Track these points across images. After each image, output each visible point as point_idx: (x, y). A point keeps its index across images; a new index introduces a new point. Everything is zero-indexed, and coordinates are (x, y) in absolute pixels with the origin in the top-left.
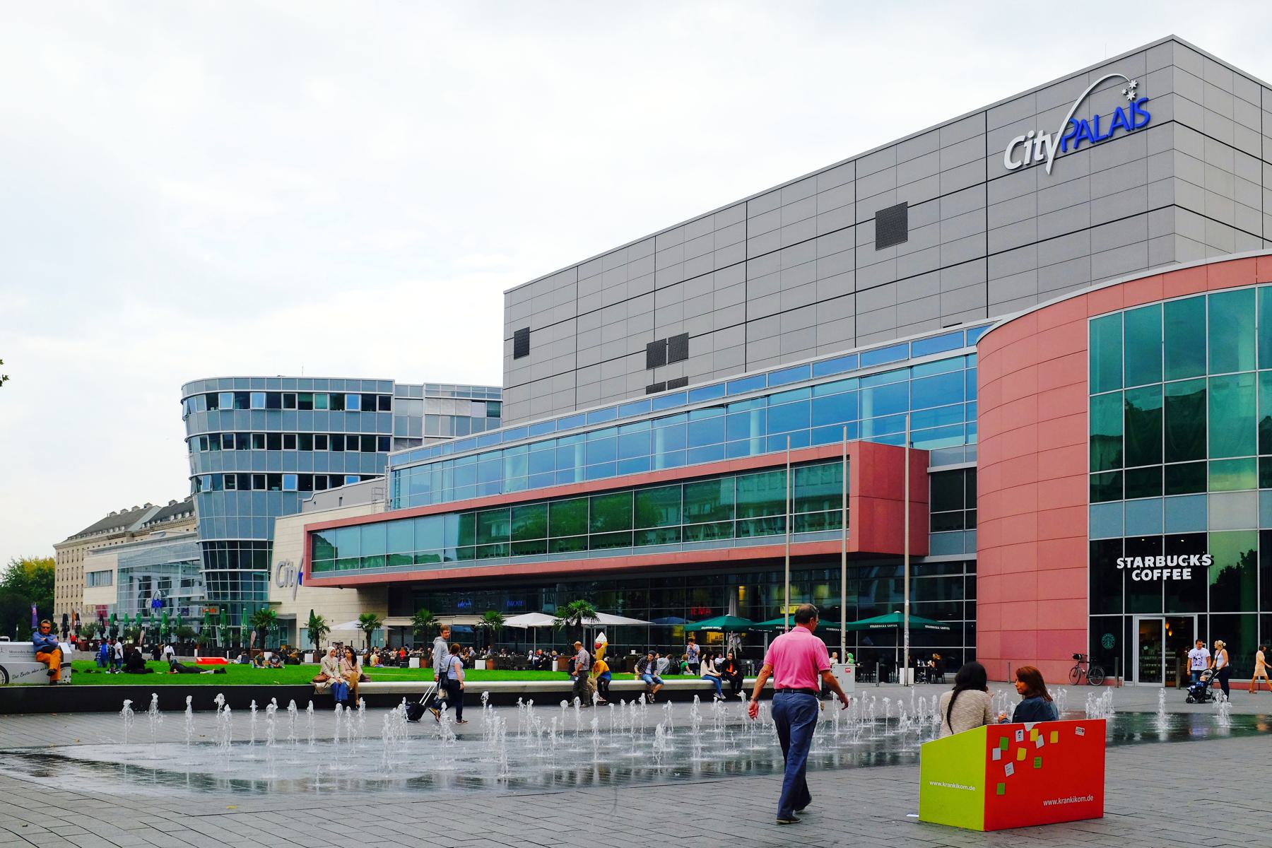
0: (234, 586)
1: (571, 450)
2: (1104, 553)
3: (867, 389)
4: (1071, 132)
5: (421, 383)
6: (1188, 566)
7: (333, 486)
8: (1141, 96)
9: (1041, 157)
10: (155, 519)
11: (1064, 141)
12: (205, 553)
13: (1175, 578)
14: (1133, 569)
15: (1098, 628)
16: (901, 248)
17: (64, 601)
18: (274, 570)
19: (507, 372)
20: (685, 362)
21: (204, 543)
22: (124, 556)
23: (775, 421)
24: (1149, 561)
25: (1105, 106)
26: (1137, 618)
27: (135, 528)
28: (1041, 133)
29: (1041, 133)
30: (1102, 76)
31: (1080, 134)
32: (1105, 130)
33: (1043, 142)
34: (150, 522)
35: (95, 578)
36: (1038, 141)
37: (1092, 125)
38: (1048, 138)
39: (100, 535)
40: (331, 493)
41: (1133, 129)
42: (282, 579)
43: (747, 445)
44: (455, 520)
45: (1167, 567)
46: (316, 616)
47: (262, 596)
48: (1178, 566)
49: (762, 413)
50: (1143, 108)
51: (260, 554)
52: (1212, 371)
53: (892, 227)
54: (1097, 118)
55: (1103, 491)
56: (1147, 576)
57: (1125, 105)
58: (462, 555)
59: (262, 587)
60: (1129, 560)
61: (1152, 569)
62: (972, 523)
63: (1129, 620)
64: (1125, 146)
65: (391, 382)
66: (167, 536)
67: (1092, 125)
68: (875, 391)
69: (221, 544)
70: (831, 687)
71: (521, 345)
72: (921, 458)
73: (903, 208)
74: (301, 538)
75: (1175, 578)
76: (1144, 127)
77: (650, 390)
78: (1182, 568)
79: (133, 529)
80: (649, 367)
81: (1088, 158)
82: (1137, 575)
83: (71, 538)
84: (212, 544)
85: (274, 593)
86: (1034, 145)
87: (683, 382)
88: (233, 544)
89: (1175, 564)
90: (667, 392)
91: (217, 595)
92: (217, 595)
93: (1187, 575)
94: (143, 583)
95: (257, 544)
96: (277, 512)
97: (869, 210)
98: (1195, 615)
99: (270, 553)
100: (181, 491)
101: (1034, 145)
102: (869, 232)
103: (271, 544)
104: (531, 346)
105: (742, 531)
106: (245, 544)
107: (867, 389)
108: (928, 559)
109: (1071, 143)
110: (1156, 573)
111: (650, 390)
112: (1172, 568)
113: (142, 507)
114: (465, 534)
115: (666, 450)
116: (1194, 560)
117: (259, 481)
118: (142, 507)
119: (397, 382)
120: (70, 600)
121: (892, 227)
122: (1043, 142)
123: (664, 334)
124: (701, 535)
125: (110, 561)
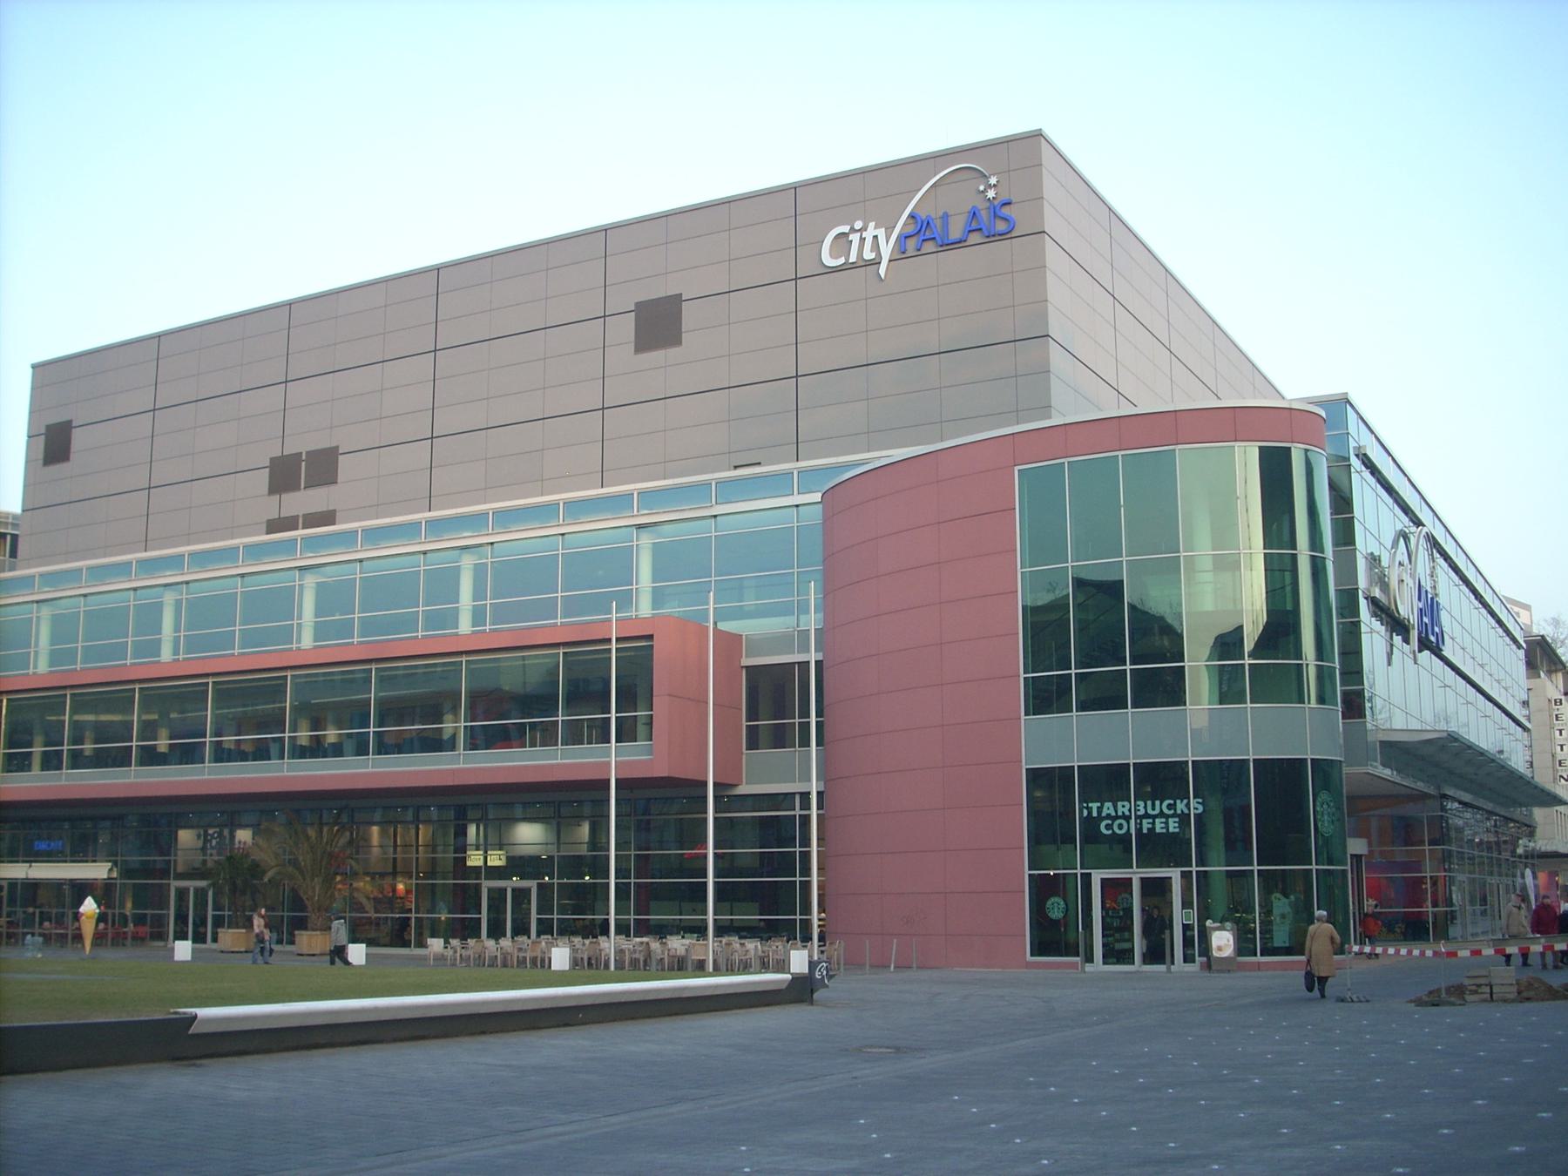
2: (1050, 787)
4: (911, 229)
7: (142, 763)
8: (1004, 197)
9: (873, 256)
13: (1158, 830)
14: (1100, 818)
15: (1043, 889)
16: (673, 352)
19: (31, 484)
20: (333, 488)
25: (959, 204)
26: (1097, 876)
28: (872, 225)
29: (872, 225)
31: (924, 234)
33: (876, 237)
36: (869, 235)
38: (881, 233)
41: (993, 237)
43: (455, 614)
45: (1146, 815)
48: (1162, 814)
49: (479, 571)
50: (1006, 211)
53: (659, 324)
54: (945, 217)
55: (1045, 698)
57: (982, 206)
60: (1094, 806)
63: (1087, 879)
64: (977, 258)
67: (939, 223)
68: (321, 588)
70: (95, 840)
71: (53, 444)
72: (729, 644)
73: (676, 300)
75: (1158, 830)
76: (1003, 236)
77: (274, 526)
78: (1167, 817)
80: (272, 491)
82: (1108, 827)
86: (862, 240)
87: (328, 518)
89: (1157, 811)
93: (1173, 826)
97: (625, 299)
98: (1174, 874)
101: (862, 240)
107: (646, 541)
108: (743, 789)
109: (911, 244)
115: (317, 616)
116: (1180, 806)
121: (659, 324)
122: (876, 237)
123: (302, 443)
124: (36, 761)
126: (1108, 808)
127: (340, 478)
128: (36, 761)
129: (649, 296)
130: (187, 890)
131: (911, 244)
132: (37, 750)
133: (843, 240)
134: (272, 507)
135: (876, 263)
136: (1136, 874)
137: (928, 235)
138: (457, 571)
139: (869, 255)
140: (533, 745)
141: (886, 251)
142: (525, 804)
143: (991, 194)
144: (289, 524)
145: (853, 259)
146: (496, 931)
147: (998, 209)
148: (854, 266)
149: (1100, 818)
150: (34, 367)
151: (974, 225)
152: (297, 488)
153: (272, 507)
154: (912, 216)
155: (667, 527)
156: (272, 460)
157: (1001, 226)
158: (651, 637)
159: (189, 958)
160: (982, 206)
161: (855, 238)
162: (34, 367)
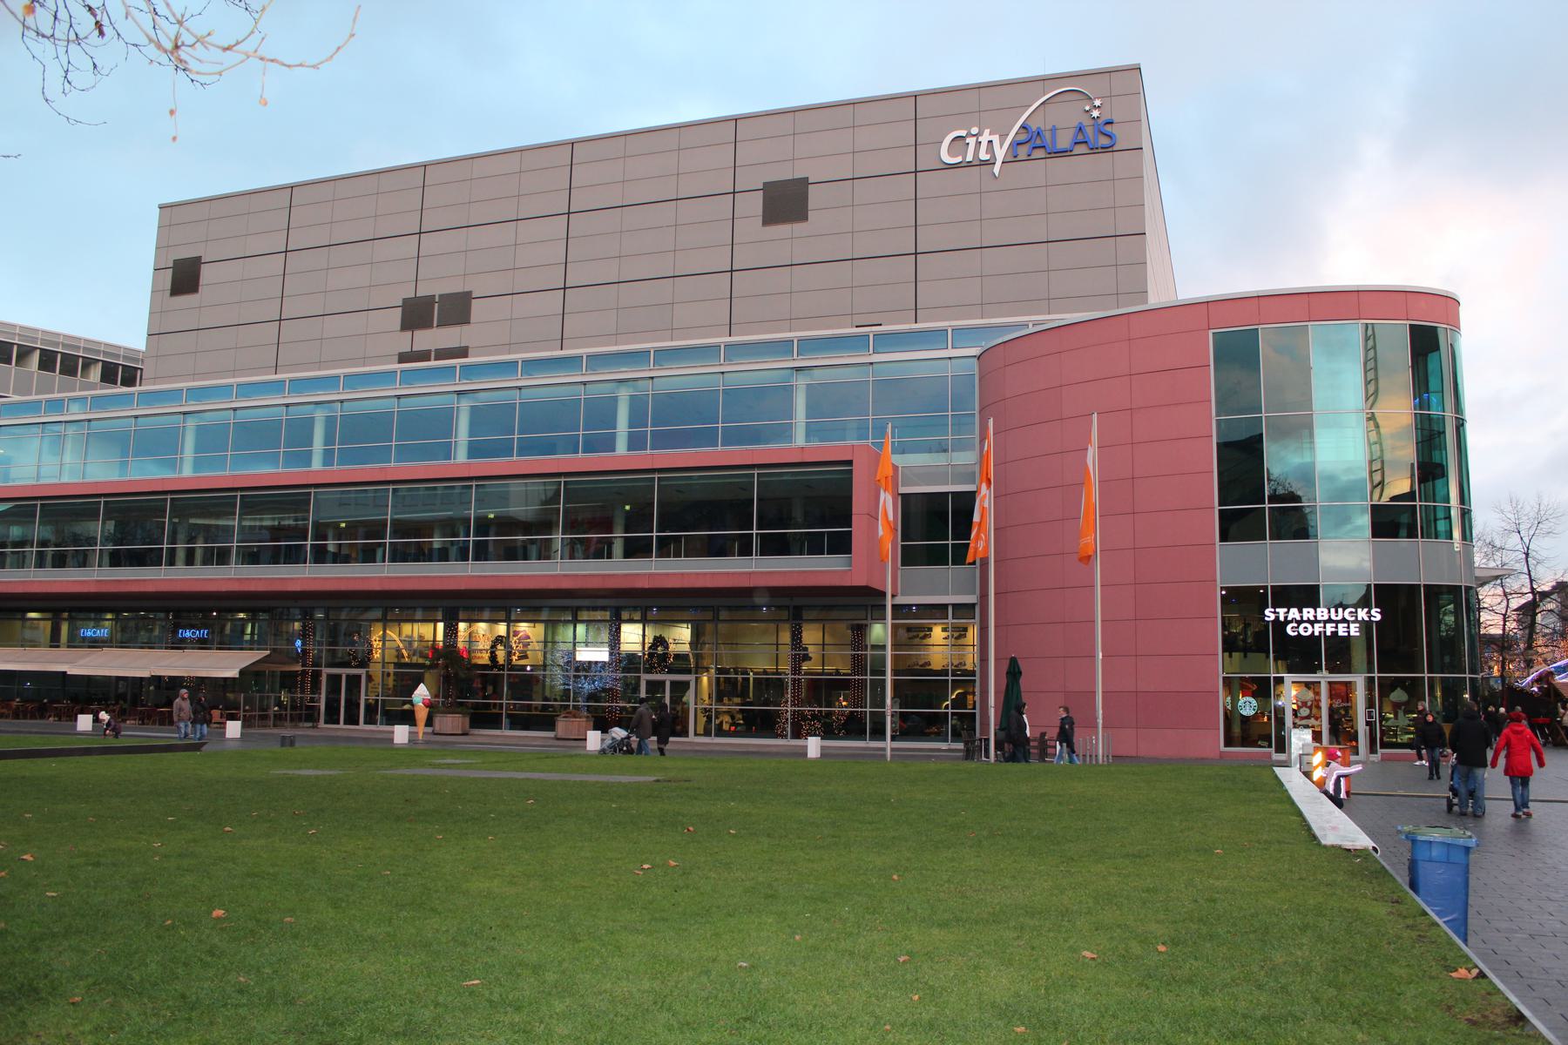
1: (310, 423)
3: (465, 405)
4: (1023, 137)
6: (1356, 621)
8: (1106, 117)
9: (987, 157)
11: (1016, 144)
14: (1287, 622)
16: (798, 227)
20: (465, 328)
23: (210, 439)
24: (1308, 613)
25: (1065, 120)
28: (987, 131)
29: (987, 131)
30: (1072, 87)
31: (1033, 143)
32: (1064, 142)
36: (984, 139)
37: (1048, 135)
38: (996, 139)
41: (1094, 150)
43: (613, 438)
45: (1330, 620)
48: (1344, 620)
49: (330, 421)
50: (1108, 129)
53: (786, 202)
54: (1054, 130)
56: (1305, 631)
60: (1282, 611)
61: (1312, 623)
62: (572, 557)
64: (1083, 165)
68: (474, 410)
71: (184, 278)
73: (805, 182)
77: (403, 358)
80: (404, 327)
81: (1039, 169)
87: (463, 352)
90: (433, 363)
93: (1354, 630)
102: (755, 204)
104: (811, 206)
107: (465, 405)
110: (1330, 629)
111: (403, 358)
112: (1337, 622)
121: (786, 202)
123: (435, 287)
124: (618, 548)
126: (1294, 613)
127: (473, 320)
128: (618, 548)
129: (779, 180)
130: (340, 676)
131: (1023, 152)
132: (618, 535)
133: (960, 143)
134: (404, 342)
135: (990, 163)
136: (668, 678)
137: (1038, 142)
138: (615, 399)
139: (984, 156)
140: (678, 555)
141: (1000, 154)
142: (425, 609)
143: (1095, 113)
144: (424, 356)
145: (969, 158)
146: (332, 717)
147: (1105, 126)
148: (970, 165)
149: (1287, 622)
151: (1080, 138)
152: (430, 326)
153: (404, 342)
154: (1023, 127)
155: (482, 394)
156: (405, 300)
157: (1104, 141)
158: (850, 463)
159: (238, 736)
160: (1087, 122)
161: (972, 141)
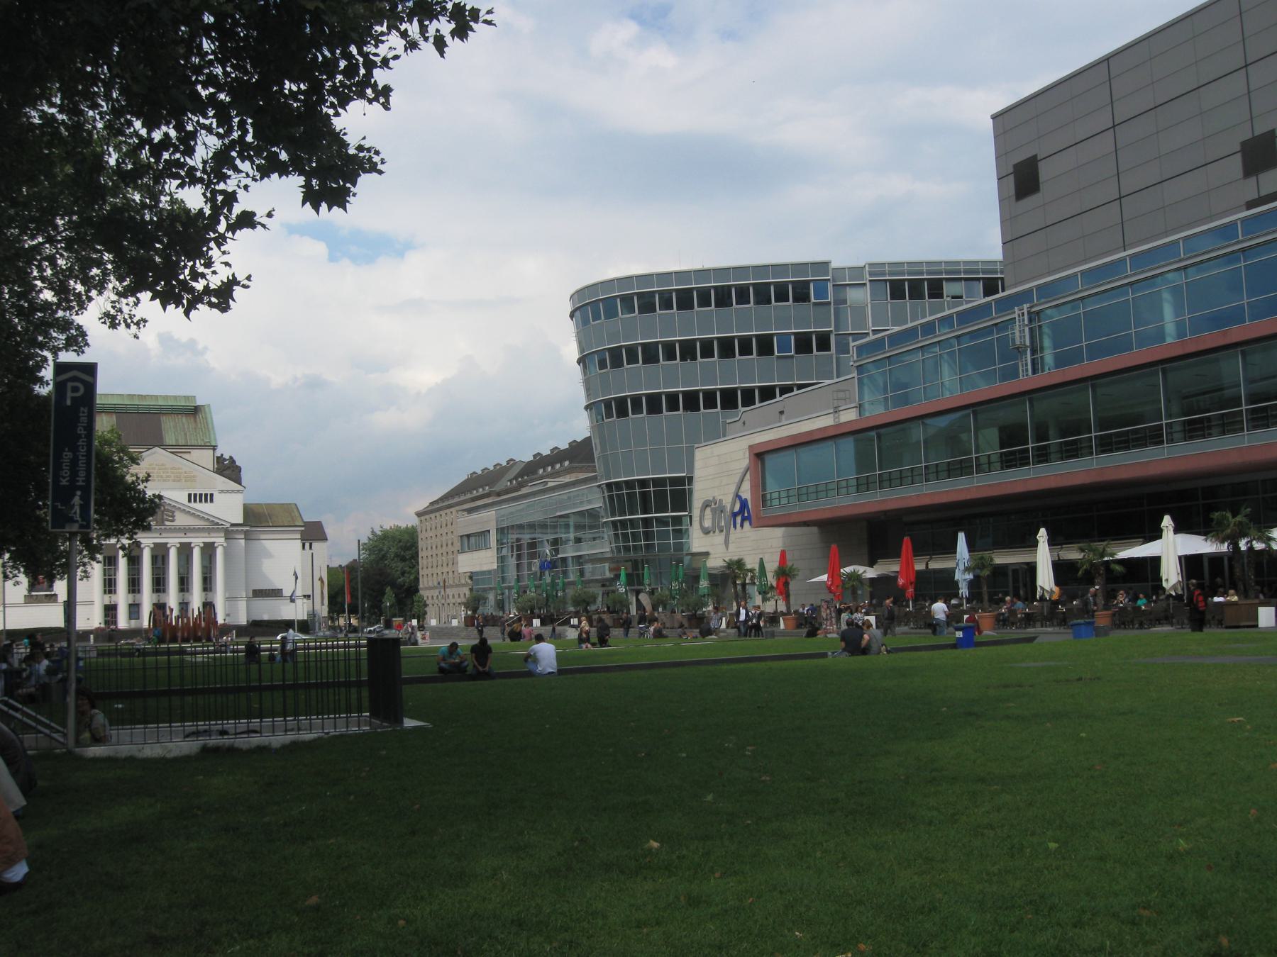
0: (648, 536)
5: (862, 264)
7: (762, 400)
10: (521, 474)
12: (611, 498)
17: (429, 572)
18: (696, 513)
19: (1006, 221)
21: (609, 486)
22: (503, 512)
27: (504, 483)
34: (516, 478)
35: (473, 541)
39: (463, 498)
40: (761, 409)
42: (708, 523)
44: (848, 445)
46: (789, 564)
47: (679, 547)
51: (676, 494)
52: (1242, 307)
58: (863, 485)
59: (679, 533)
65: (827, 264)
66: (550, 485)
69: (629, 484)
71: (1022, 180)
74: (744, 461)
79: (497, 488)
83: (432, 504)
84: (618, 485)
85: (697, 542)
88: (643, 483)
91: (627, 549)
92: (627, 549)
94: (520, 543)
95: (675, 481)
96: (696, 439)
99: (691, 491)
100: (580, 427)
103: (691, 479)
104: (1041, 180)
105: (1043, 456)
106: (658, 482)
113: (504, 464)
114: (863, 462)
117: (672, 401)
118: (504, 464)
119: (834, 265)
120: (439, 571)
125: (488, 519)
134: (1250, 189)
150: (994, 117)
162: (994, 117)
